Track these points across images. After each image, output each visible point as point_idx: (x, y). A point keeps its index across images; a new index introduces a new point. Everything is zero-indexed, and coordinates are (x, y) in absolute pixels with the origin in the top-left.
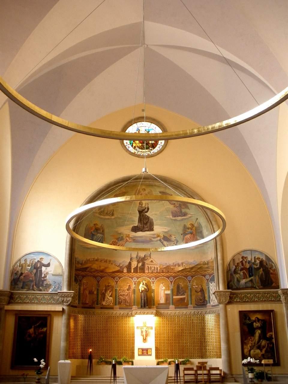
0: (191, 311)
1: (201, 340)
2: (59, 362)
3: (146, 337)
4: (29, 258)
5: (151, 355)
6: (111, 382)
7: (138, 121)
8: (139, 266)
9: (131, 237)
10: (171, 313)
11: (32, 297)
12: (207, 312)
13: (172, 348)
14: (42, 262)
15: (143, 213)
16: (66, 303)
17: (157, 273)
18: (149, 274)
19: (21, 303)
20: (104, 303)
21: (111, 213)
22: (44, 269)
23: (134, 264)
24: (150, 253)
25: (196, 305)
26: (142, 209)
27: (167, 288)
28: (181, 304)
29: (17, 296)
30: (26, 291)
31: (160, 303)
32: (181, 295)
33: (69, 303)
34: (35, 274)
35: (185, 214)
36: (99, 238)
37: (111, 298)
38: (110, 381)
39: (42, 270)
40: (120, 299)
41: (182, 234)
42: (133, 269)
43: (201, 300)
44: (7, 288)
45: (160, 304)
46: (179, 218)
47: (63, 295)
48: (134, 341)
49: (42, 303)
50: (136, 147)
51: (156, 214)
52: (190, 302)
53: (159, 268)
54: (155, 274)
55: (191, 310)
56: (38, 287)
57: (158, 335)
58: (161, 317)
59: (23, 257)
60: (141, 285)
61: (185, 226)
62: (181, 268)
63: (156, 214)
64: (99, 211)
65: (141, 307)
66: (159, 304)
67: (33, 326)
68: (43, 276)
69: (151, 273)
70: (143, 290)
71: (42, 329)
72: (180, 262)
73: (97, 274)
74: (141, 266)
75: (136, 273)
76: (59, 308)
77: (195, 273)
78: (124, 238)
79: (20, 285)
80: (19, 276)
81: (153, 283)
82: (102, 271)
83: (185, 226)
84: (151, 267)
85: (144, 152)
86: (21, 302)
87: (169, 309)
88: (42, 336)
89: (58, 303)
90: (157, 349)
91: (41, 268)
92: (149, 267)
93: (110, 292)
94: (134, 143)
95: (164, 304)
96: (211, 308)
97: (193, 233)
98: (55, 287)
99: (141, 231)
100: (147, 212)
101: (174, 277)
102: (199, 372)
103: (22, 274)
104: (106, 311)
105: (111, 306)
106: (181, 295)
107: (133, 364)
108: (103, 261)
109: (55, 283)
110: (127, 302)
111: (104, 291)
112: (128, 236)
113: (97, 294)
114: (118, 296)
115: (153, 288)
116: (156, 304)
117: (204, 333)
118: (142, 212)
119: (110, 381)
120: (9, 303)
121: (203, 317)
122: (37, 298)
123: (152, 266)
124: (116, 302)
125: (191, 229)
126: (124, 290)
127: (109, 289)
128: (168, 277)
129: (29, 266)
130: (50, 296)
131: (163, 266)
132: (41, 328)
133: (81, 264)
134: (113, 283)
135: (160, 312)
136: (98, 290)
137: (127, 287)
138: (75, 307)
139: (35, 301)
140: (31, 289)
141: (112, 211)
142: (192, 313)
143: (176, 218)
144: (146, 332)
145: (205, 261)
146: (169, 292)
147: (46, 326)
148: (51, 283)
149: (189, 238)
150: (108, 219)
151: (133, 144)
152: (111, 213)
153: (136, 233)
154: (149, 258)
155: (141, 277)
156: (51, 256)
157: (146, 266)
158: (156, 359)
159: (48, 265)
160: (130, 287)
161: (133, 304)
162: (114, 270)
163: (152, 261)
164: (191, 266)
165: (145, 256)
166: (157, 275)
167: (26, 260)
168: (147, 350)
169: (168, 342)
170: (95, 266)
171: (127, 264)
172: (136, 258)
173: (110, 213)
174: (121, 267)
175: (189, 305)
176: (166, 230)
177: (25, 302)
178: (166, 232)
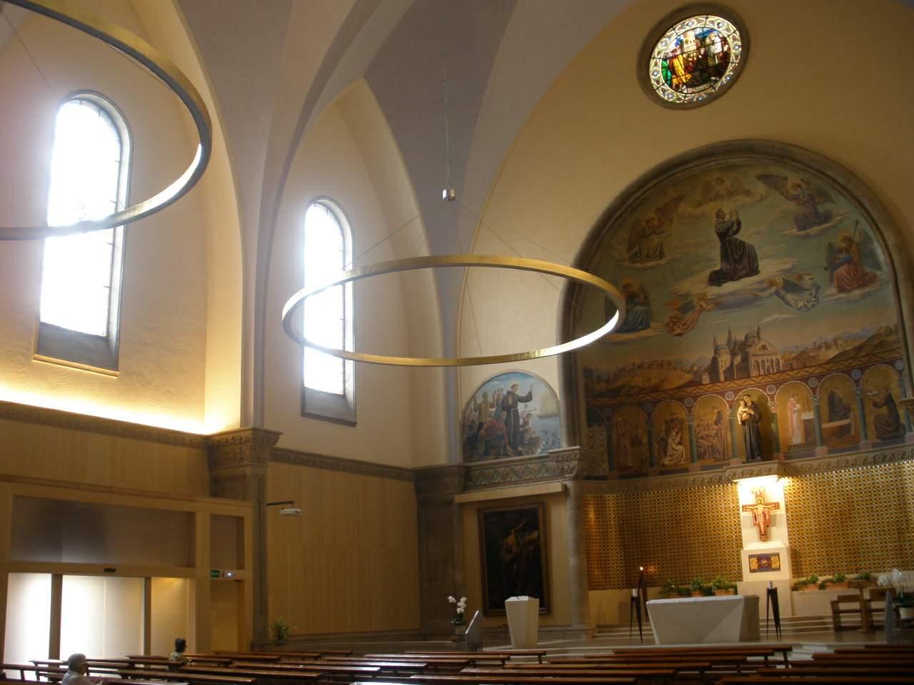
0: (867, 455)
1: (898, 525)
2: (507, 600)
3: (764, 528)
4: (490, 389)
5: (778, 569)
6: (631, 635)
7: (675, 21)
8: (736, 363)
9: (711, 300)
10: (819, 465)
11: (505, 470)
12: (907, 454)
13: (829, 549)
14: (516, 393)
15: (730, 236)
16: (569, 474)
17: (777, 373)
18: (761, 378)
19: (486, 486)
20: (667, 461)
21: (657, 253)
22: (521, 406)
23: (725, 361)
24: (759, 329)
25: (878, 437)
26: (726, 226)
27: (806, 406)
28: (840, 441)
29: (477, 473)
30: (493, 459)
31: (793, 444)
32: (841, 419)
33: (575, 472)
34: (506, 423)
35: (827, 218)
36: (639, 316)
37: (681, 448)
38: (629, 633)
39: (517, 410)
40: (700, 447)
41: (826, 269)
42: (724, 372)
43: (889, 425)
44: (457, 459)
45: (791, 446)
46: (816, 229)
47: (558, 457)
48: (741, 540)
49: (527, 481)
50: (681, 85)
51: (759, 233)
52: (862, 434)
53: (781, 362)
54: (775, 377)
55: (867, 452)
56: (515, 448)
57: (795, 521)
58: (797, 477)
59: (479, 389)
60: (741, 409)
61: (831, 245)
62: (832, 353)
63: (759, 233)
64: (630, 254)
65: (748, 459)
66: (789, 447)
67: (513, 531)
68: (521, 422)
69: (765, 375)
70: (748, 420)
71: (530, 534)
72: (829, 337)
73: (643, 397)
74: (739, 364)
75: (731, 380)
76: (555, 487)
77: (869, 360)
78: (695, 304)
79: (482, 448)
80: (476, 429)
81: (772, 399)
82: (655, 389)
83: (831, 245)
84: (763, 361)
85: (699, 92)
86: (485, 485)
87: (814, 456)
88: (531, 547)
89: (556, 476)
90: (795, 555)
91: (516, 406)
92: (758, 363)
93: (677, 433)
94: (674, 76)
95: (803, 444)
96: (827, 456)
97: (852, 261)
98: (547, 443)
99: (732, 279)
100: (738, 230)
101: (819, 377)
102: (875, 605)
103: (481, 425)
104: (673, 478)
105: (682, 464)
106: (841, 419)
107: (736, 593)
108: (654, 367)
109: (546, 433)
110: (718, 451)
111: (663, 434)
112: (703, 297)
113: (650, 444)
114: (695, 439)
115: (773, 410)
116: (783, 449)
117: (905, 508)
118: (727, 235)
119: (629, 633)
120: (465, 488)
121: (899, 468)
122: (515, 473)
123: (765, 358)
124: (692, 456)
125: (848, 251)
126: (708, 425)
127: (673, 428)
128: (805, 380)
129: (492, 406)
130: (539, 462)
131: (790, 354)
132: (528, 533)
133: (607, 382)
134: (682, 414)
135: (792, 467)
136: (650, 434)
137: (715, 418)
138: (604, 478)
139: (511, 478)
140: (502, 453)
141: (659, 248)
142: (869, 460)
143: (808, 231)
144: (765, 516)
145: (890, 326)
146: (809, 415)
147: (537, 528)
148: (538, 434)
149: (845, 273)
150: (653, 267)
151: (671, 79)
152: (657, 253)
153: (719, 288)
154: (756, 340)
155: (744, 389)
156: (530, 376)
157: (752, 360)
158: (794, 577)
159: (528, 398)
160: (722, 416)
161: (730, 453)
162: (681, 382)
163: (764, 347)
164: (857, 344)
165: (747, 337)
166: (779, 377)
167: (485, 395)
168: (767, 557)
169: (819, 535)
170: (638, 381)
171: (708, 363)
172: (728, 345)
173: (654, 253)
174: (695, 373)
175: (862, 442)
176: (788, 266)
177: (493, 484)
178: (787, 271)
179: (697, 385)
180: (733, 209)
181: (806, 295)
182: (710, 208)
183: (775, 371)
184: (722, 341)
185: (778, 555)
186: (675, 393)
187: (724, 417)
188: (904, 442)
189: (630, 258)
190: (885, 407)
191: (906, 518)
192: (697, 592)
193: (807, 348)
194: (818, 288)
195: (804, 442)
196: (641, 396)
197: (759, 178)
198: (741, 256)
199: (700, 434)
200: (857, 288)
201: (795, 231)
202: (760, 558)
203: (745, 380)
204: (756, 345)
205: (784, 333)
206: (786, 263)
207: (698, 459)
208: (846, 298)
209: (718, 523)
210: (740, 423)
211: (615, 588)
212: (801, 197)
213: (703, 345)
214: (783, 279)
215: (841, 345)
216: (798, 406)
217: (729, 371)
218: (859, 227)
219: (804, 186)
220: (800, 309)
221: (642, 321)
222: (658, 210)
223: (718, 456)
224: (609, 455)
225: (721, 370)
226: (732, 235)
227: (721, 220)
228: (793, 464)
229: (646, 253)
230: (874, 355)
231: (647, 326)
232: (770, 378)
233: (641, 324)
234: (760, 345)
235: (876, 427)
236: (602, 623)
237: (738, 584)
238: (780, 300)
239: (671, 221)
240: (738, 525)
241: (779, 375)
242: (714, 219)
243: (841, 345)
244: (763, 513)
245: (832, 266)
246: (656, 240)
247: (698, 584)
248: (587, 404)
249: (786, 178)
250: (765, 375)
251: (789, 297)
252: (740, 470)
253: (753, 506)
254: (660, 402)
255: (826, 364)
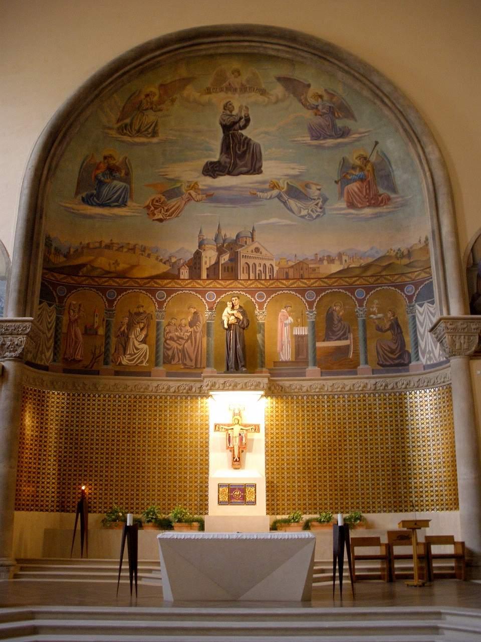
0: (366, 381)
3: (239, 453)
5: (254, 503)
8: (222, 261)
9: (202, 190)
15: (234, 130)
17: (270, 279)
18: (249, 282)
20: (125, 361)
21: (150, 130)
23: (209, 257)
24: (253, 230)
26: (232, 119)
27: (299, 320)
32: (339, 339)
33: (20, 350)
35: (345, 133)
40: (168, 349)
41: (336, 182)
42: (207, 269)
43: (392, 352)
46: (330, 142)
51: (266, 133)
60: (228, 310)
62: (335, 268)
64: (119, 124)
66: (276, 363)
69: (255, 279)
72: (334, 251)
75: (215, 280)
81: (261, 308)
82: (122, 275)
90: (271, 488)
93: (142, 329)
95: (292, 362)
99: (229, 173)
100: (245, 127)
101: (318, 291)
104: (131, 381)
107: (202, 528)
108: (125, 250)
111: (124, 328)
112: (194, 186)
114: (163, 340)
123: (257, 262)
124: (157, 358)
125: (362, 169)
126: (180, 325)
127: (138, 323)
128: (302, 292)
136: (108, 325)
138: (46, 368)
141: (154, 125)
144: (241, 439)
146: (303, 331)
149: (356, 190)
150: (143, 144)
152: (150, 130)
154: (249, 241)
155: (229, 291)
157: (242, 262)
162: (155, 272)
163: (257, 250)
164: (363, 262)
165: (237, 236)
168: (243, 488)
170: (103, 262)
171: (190, 256)
173: (147, 130)
175: (361, 367)
176: (295, 172)
178: (295, 177)
179: (174, 279)
180: (244, 104)
181: (312, 204)
182: (219, 99)
183: (268, 278)
184: (210, 235)
185: (254, 486)
186: (145, 284)
187: (201, 318)
188: (408, 371)
189: (118, 129)
190: (389, 332)
191: (403, 454)
192: (150, 524)
193: (307, 259)
194: (325, 200)
195: (294, 360)
196: (104, 280)
197: (279, 79)
198: (244, 153)
199: (171, 335)
200: (369, 206)
201: (308, 139)
202: (232, 488)
203: (230, 282)
204: (249, 246)
205: (282, 239)
206: (293, 169)
207: (164, 363)
208: (357, 215)
209: (181, 442)
210: (226, 326)
211: (42, 510)
212: (320, 108)
213: (186, 235)
214: (288, 184)
215: (346, 261)
216: (290, 318)
217: (213, 272)
218: (377, 147)
219: (326, 97)
220: (303, 217)
221: (119, 196)
222: (161, 85)
223: (188, 362)
224: (56, 343)
225: (204, 267)
226: (237, 130)
227: (228, 112)
228: (281, 383)
229: (137, 128)
230: (382, 276)
231: (124, 204)
232: (262, 284)
233: (117, 200)
234: (253, 247)
235: (378, 353)
236: (22, 557)
237: (205, 518)
238: (282, 204)
239: (173, 101)
240: (205, 446)
241: (271, 282)
242: (221, 110)
243: (346, 261)
244: (240, 435)
245: (343, 180)
246: (151, 117)
247: (154, 513)
248: (43, 278)
249: (309, 86)
250: (255, 279)
251: (292, 203)
252: (222, 381)
253: (229, 425)
254: (126, 290)
255: (325, 278)
